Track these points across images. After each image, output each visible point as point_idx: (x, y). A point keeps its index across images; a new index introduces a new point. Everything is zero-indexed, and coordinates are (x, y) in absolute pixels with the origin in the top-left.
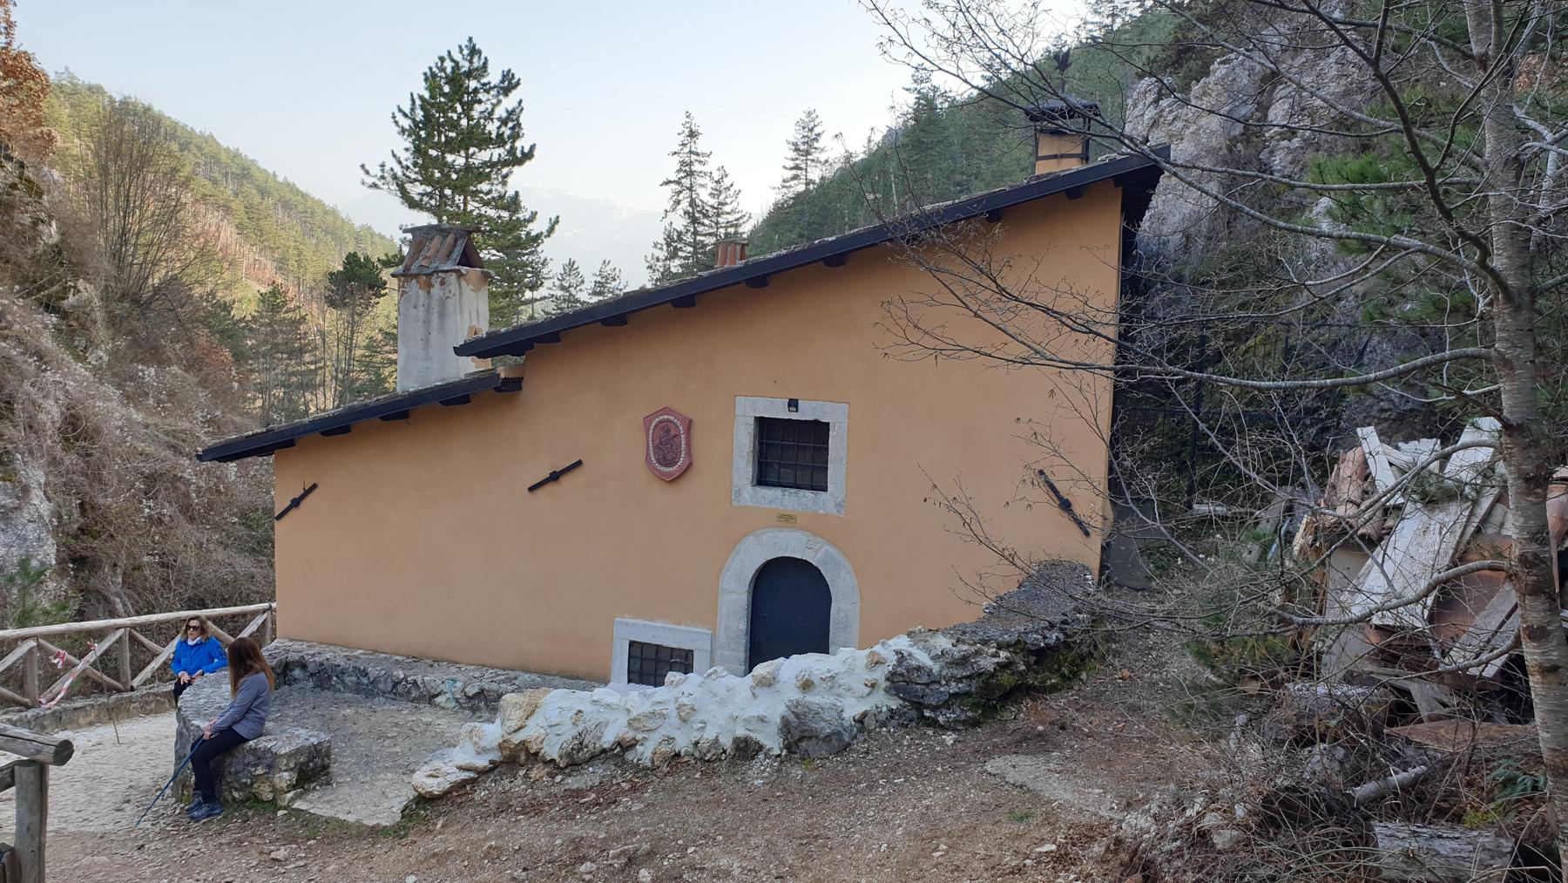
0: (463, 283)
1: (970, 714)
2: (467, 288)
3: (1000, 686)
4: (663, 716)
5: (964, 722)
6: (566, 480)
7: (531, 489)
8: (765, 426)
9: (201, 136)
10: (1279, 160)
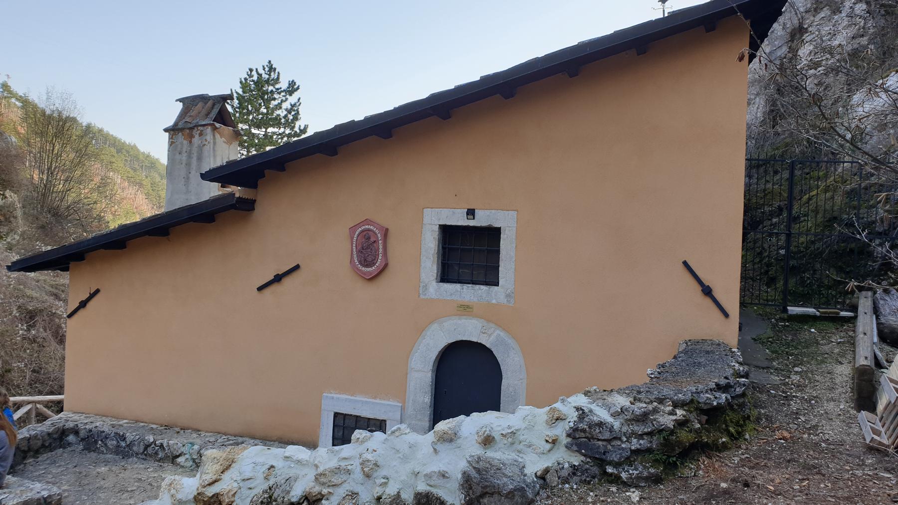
0: (217, 136)
1: (652, 470)
2: (220, 140)
3: (679, 443)
4: (349, 472)
5: (646, 479)
6: (287, 282)
7: (260, 289)
8: (448, 232)
9: (129, 145)
10: (810, 84)
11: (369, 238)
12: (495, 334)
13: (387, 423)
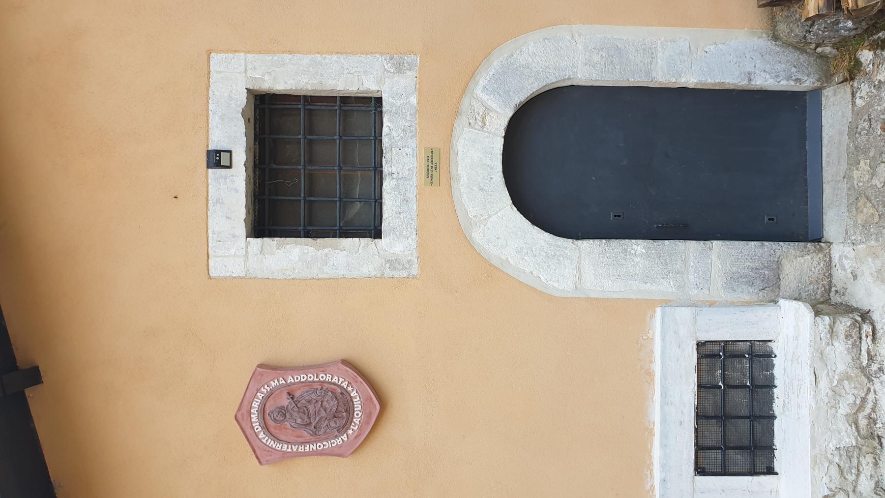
8: (269, 218)
11: (283, 411)
12: (484, 97)
13: (704, 337)
